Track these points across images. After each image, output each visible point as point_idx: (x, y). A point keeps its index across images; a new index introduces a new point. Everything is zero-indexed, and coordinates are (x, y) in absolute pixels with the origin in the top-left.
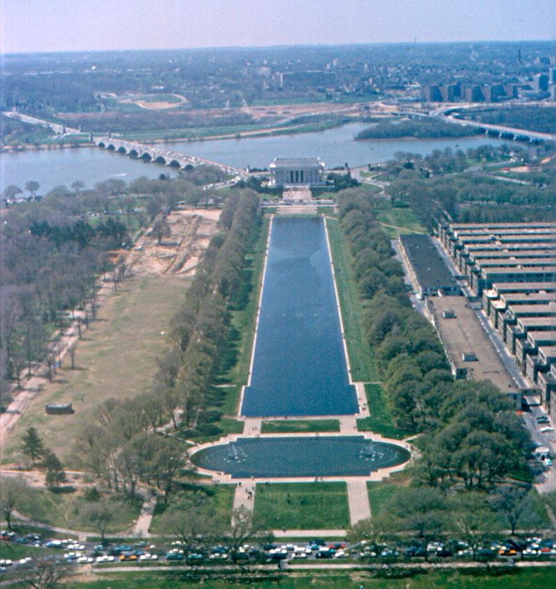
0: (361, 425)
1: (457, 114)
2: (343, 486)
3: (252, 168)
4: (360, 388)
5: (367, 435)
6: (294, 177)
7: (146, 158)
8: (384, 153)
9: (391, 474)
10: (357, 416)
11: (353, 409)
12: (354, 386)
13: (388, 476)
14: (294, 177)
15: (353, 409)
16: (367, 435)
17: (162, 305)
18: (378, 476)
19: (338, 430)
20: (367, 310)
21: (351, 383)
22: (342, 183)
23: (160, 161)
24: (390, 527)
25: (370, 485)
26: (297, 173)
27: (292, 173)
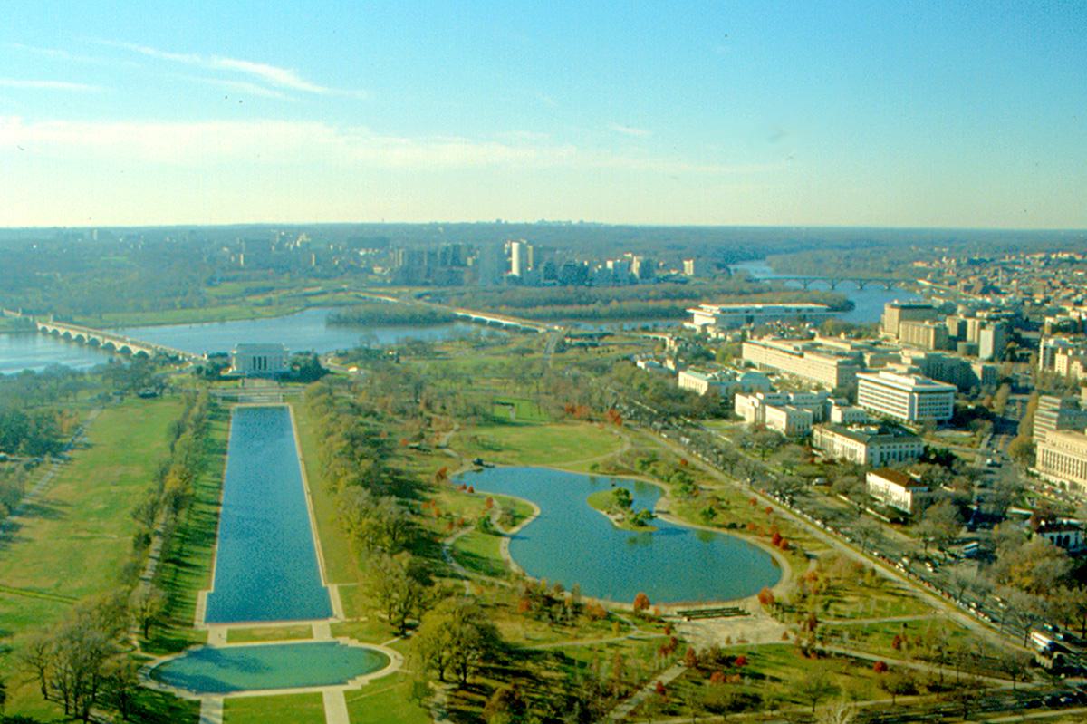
0: (336, 631)
1: (428, 298)
2: (320, 695)
3: (210, 353)
4: (334, 592)
5: (343, 640)
6: (263, 363)
7: (94, 343)
8: (350, 339)
9: (371, 681)
10: (332, 620)
11: (327, 613)
12: (326, 589)
13: (350, 682)
14: (263, 363)
15: (327, 613)
16: (343, 640)
17: (406, 290)
18: (353, 685)
19: (311, 637)
20: (542, 411)
21: (324, 585)
22: (310, 371)
23: (110, 348)
24: (796, 695)
25: (347, 693)
26: (260, 359)
27: (254, 359)
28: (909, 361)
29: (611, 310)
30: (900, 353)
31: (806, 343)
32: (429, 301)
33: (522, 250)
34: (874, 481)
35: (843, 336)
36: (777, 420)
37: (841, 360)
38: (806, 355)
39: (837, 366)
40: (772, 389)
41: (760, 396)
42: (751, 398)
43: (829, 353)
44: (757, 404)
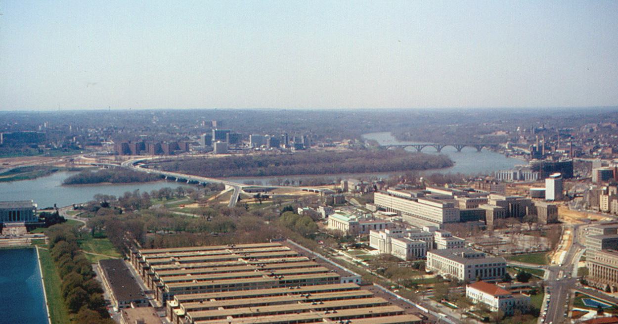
6: (509, 175)
14: (509, 175)
22: (51, 220)
28: (495, 203)
29: (153, 157)
30: (488, 197)
31: (419, 191)
32: (143, 167)
33: (512, 205)
34: (472, 292)
35: (446, 186)
36: (400, 249)
37: (541, 277)
38: (420, 200)
39: (444, 208)
40: (398, 229)
41: (387, 231)
42: (381, 233)
43: (437, 198)
44: (385, 237)
